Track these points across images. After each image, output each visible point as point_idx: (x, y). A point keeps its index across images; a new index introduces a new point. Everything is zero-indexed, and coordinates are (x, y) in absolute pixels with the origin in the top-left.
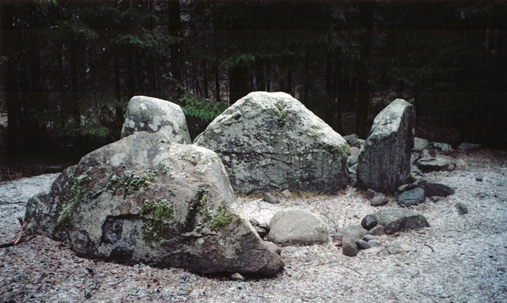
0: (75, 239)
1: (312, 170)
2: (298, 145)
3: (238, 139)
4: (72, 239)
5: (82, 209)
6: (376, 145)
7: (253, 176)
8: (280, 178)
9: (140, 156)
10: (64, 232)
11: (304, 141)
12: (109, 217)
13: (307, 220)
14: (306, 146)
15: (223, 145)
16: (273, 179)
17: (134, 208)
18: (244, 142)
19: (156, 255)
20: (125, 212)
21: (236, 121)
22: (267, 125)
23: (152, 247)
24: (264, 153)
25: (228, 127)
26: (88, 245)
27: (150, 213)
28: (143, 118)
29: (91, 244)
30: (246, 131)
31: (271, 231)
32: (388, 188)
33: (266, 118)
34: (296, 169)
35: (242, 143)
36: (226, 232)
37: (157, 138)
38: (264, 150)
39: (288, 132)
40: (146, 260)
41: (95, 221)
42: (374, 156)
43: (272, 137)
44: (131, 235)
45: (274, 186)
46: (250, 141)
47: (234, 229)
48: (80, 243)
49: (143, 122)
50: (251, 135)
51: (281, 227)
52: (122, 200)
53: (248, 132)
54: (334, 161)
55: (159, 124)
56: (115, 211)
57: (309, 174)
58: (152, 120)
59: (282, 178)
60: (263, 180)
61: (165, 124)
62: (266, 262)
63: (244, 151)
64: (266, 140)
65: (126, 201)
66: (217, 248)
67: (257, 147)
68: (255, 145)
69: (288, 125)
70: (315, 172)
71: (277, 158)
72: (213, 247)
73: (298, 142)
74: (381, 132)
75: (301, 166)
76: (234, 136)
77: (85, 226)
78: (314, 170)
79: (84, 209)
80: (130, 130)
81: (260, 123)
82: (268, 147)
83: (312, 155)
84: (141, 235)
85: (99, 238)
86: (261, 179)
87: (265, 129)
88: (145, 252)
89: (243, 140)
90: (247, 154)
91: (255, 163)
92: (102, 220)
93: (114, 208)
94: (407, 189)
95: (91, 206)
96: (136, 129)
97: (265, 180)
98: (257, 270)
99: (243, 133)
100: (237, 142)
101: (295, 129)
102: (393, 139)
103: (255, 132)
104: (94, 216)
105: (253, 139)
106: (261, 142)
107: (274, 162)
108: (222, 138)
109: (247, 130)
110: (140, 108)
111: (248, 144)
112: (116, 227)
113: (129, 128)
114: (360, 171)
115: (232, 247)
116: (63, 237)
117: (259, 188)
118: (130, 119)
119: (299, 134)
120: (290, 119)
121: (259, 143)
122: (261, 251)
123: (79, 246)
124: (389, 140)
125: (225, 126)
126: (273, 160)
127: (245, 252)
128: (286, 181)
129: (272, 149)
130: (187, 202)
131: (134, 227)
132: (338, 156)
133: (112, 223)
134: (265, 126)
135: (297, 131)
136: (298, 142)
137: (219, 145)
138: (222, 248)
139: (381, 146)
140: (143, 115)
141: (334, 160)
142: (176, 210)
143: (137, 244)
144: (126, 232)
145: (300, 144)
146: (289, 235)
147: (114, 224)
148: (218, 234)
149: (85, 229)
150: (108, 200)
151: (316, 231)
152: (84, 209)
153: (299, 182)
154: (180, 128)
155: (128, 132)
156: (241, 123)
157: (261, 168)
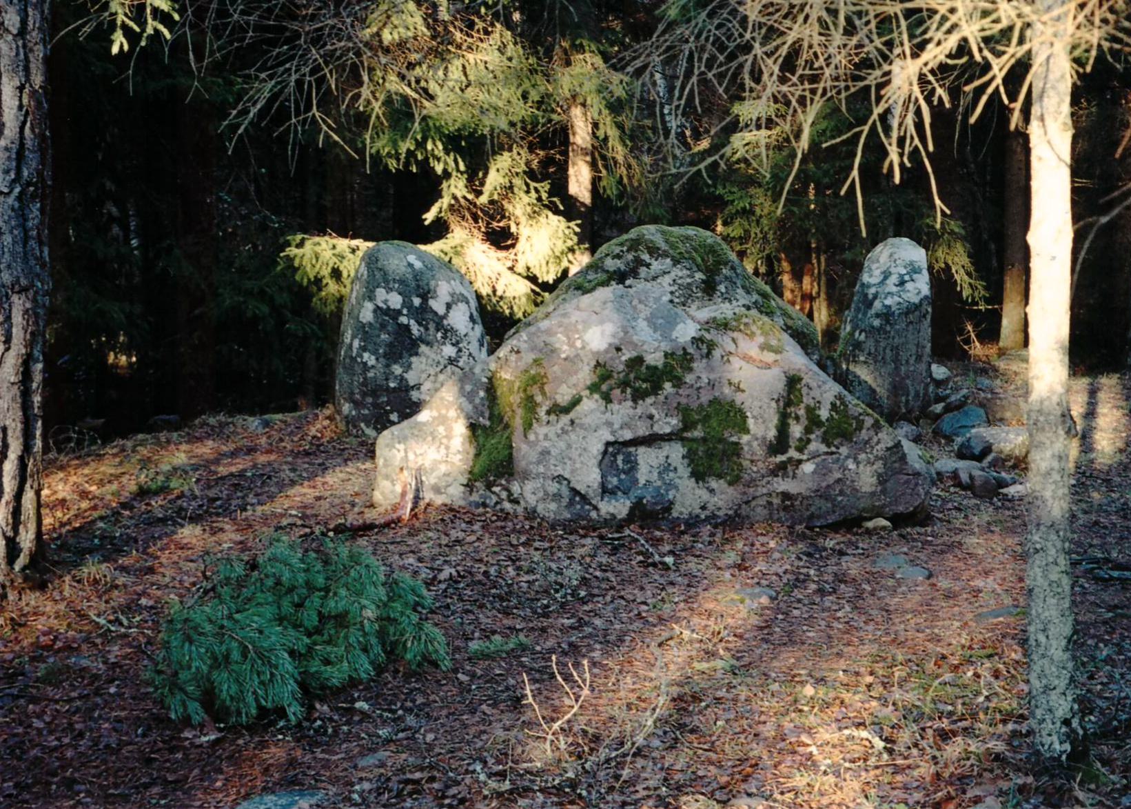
5: (541, 437)
20: (642, 430)
23: (712, 491)
27: (695, 429)
28: (418, 286)
41: (580, 455)
42: (885, 349)
47: (870, 439)
52: (631, 412)
55: (448, 299)
65: (639, 411)
69: (723, 290)
72: (838, 475)
74: (897, 299)
79: (546, 435)
84: (684, 471)
92: (595, 452)
93: (616, 426)
95: (562, 429)
96: (405, 311)
110: (410, 265)
112: (625, 461)
113: (388, 308)
120: (726, 278)
123: (553, 506)
124: (917, 313)
133: (614, 455)
135: (740, 303)
142: (754, 417)
147: (620, 458)
150: (599, 414)
152: (546, 435)
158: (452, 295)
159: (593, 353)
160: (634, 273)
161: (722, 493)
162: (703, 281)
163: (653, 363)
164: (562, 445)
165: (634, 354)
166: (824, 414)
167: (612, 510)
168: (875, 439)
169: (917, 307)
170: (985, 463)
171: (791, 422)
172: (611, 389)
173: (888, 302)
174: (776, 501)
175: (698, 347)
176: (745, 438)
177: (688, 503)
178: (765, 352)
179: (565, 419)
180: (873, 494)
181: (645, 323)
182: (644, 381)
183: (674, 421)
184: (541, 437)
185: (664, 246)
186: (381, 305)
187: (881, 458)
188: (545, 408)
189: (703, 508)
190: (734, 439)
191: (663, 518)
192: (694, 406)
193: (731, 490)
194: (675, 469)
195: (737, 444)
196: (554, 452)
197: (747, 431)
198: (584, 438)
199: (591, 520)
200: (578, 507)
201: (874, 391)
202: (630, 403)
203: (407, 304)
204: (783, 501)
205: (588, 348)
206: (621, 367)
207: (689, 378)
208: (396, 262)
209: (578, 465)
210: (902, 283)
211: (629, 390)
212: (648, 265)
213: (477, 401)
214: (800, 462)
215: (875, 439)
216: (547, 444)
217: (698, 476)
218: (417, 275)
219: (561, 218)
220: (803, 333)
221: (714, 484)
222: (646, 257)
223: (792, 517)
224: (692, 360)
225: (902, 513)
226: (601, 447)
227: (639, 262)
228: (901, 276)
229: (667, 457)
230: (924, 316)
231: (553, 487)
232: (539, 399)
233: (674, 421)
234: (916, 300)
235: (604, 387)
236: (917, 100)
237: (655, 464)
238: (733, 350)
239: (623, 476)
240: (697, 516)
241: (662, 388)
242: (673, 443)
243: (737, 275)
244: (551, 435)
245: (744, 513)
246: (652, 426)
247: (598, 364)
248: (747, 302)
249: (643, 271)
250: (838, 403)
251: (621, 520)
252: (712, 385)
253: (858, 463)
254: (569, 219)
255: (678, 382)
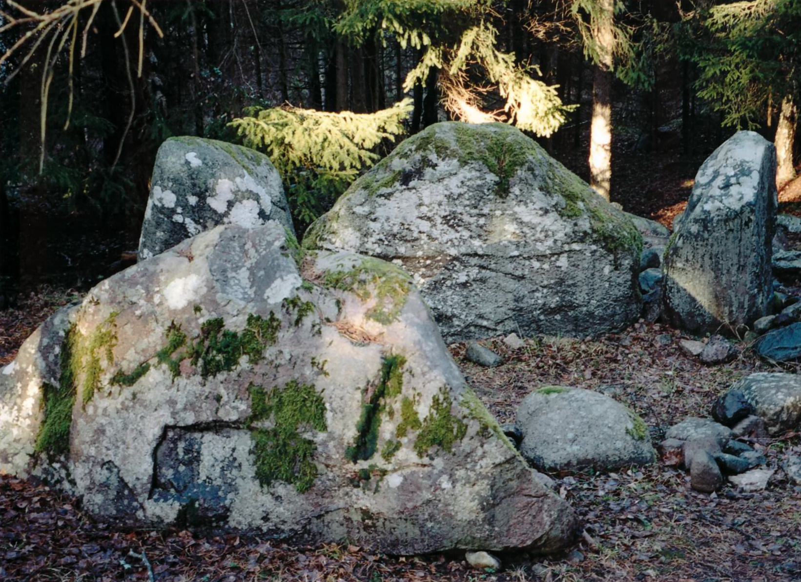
0: (88, 482)
1: (569, 289)
2: (538, 235)
3: (406, 226)
4: (78, 481)
5: (100, 411)
6: (708, 231)
7: (440, 307)
8: (499, 310)
9: (232, 283)
10: (57, 465)
11: (552, 228)
12: (166, 428)
13: (606, 412)
14: (556, 237)
15: (373, 239)
16: (482, 311)
17: (227, 407)
18: (420, 232)
19: (287, 514)
20: (206, 416)
21: (404, 187)
22: (471, 194)
23: (278, 498)
24: (464, 255)
25: (386, 201)
26: (119, 497)
28: (194, 185)
29: (126, 492)
30: (424, 209)
31: (526, 440)
32: (731, 323)
33: (469, 180)
34: (535, 288)
35: (416, 235)
36: (455, 459)
37: (269, 238)
38: (463, 250)
39: (517, 209)
40: (265, 529)
41: (135, 439)
42: (703, 257)
43: (482, 221)
44: (223, 469)
45: (485, 327)
46: (433, 229)
48: (99, 491)
49: (193, 195)
50: (436, 217)
51: (549, 431)
53: (430, 211)
54: (616, 269)
55: (230, 197)
56: (182, 415)
57: (562, 299)
58: (214, 190)
59: (503, 309)
60: (461, 314)
61: (243, 197)
62: (549, 523)
63: (420, 253)
64: (467, 227)
65: (207, 389)
66: (436, 496)
67: (450, 243)
68: (446, 238)
69: (518, 192)
70: (574, 294)
71: (493, 266)
72: (427, 495)
73: (539, 229)
74: (717, 204)
75: (545, 283)
76: (400, 220)
77: (110, 452)
78: (574, 289)
79: (105, 410)
80: (165, 211)
81: (456, 191)
82: (473, 242)
83: (569, 257)
84: (249, 470)
85: (146, 478)
86: (456, 312)
87: (467, 202)
88: (261, 509)
89: (418, 227)
90: (428, 258)
91: (443, 279)
92: (151, 437)
93: (179, 406)
94: (774, 325)
95: (123, 403)
96: (179, 210)
97: (465, 313)
98: (529, 542)
99: (419, 212)
100: (405, 232)
101: (531, 202)
102: (745, 219)
103: (445, 211)
104: (131, 426)
105: (440, 227)
106: (457, 231)
107: (486, 273)
108: (372, 225)
109: (428, 207)
110: (188, 163)
111: (430, 237)
112: (187, 451)
113: (163, 207)
114: (671, 288)
115: (471, 493)
116: (53, 476)
117: (452, 330)
118: (164, 188)
119: (541, 212)
120: (521, 180)
121: (452, 234)
122: (535, 499)
123: (99, 499)
125: (378, 199)
126: (483, 271)
127: (500, 502)
128: (511, 314)
129: (481, 246)
130: (359, 388)
131: (228, 451)
132: (624, 258)
133: (175, 442)
134: (466, 196)
136: (539, 229)
137: (366, 240)
138: (447, 497)
139: (720, 233)
140: (193, 179)
141: (617, 267)
142: (332, 410)
143: (240, 492)
144: (211, 463)
145: (543, 234)
146: (569, 449)
147: (181, 445)
148: (434, 463)
149: (112, 458)
150: (162, 389)
151: (629, 438)
153: (539, 315)
154: (273, 203)
155: (162, 216)
156: (414, 191)
157: (458, 289)
158: (235, 193)
159: (170, 311)
160: (418, 173)
161: (290, 502)
162: (497, 183)
163: (232, 329)
164: (119, 423)
165: (214, 316)
166: (423, 410)
167: (158, 511)
168: (480, 452)
169: (738, 214)
170: (738, 429)
171: (384, 417)
172: (182, 359)
173: (707, 207)
174: (357, 517)
175: (288, 312)
176: (321, 436)
177: (247, 511)
178: (371, 322)
179: (127, 392)
180: (472, 523)
181: (247, 274)
182: (219, 351)
183: (243, 407)
184: (100, 411)
185: (453, 146)
186: (157, 203)
187: (485, 477)
188: (109, 376)
189: (266, 519)
190: (307, 436)
191: (218, 527)
192: (269, 389)
193: (300, 500)
194: (240, 465)
195: (310, 442)
196: (109, 431)
197: (325, 428)
198: (142, 417)
199: (137, 520)
200: (126, 502)
201: (693, 300)
202: (199, 378)
203: (182, 202)
204: (363, 520)
205: (166, 304)
206: (197, 332)
207: (270, 352)
208: (174, 160)
209: (131, 451)
210: (727, 186)
211: (200, 362)
212: (434, 166)
213: (51, 358)
214: (384, 473)
215: (480, 452)
216: (103, 421)
217: (265, 478)
218: (193, 175)
219: (541, 83)
220: (612, 237)
221: (281, 489)
222: (433, 157)
223: (374, 539)
224: (276, 329)
225: (515, 548)
226: (157, 431)
227: (426, 162)
228: (728, 178)
229: (234, 450)
230: (747, 224)
231: (101, 475)
232: (104, 363)
233: (243, 407)
234: (737, 207)
235: (174, 356)
236: (146, 19)
237: (219, 457)
238: (332, 318)
239: (182, 468)
240: (259, 529)
241: (236, 363)
242: (242, 433)
243: (535, 176)
244: (112, 410)
245: (315, 529)
246: (217, 410)
247: (173, 326)
248: (544, 205)
249: (428, 171)
250: (441, 397)
251: (168, 524)
252: (293, 362)
253: (454, 482)
254: (549, 84)
255: (257, 356)
